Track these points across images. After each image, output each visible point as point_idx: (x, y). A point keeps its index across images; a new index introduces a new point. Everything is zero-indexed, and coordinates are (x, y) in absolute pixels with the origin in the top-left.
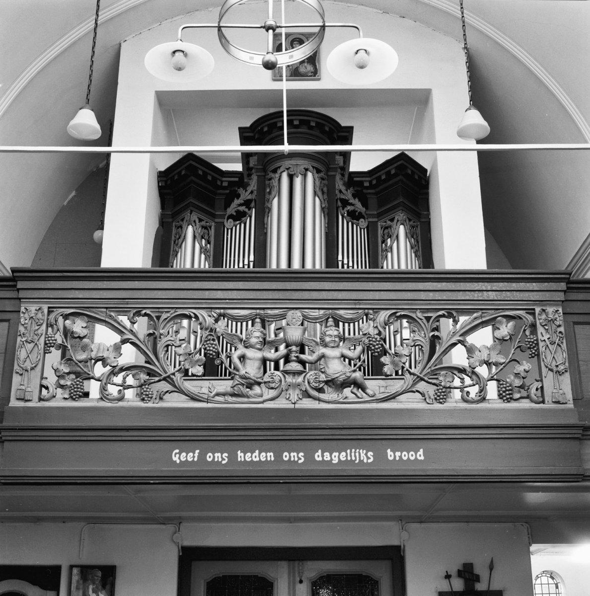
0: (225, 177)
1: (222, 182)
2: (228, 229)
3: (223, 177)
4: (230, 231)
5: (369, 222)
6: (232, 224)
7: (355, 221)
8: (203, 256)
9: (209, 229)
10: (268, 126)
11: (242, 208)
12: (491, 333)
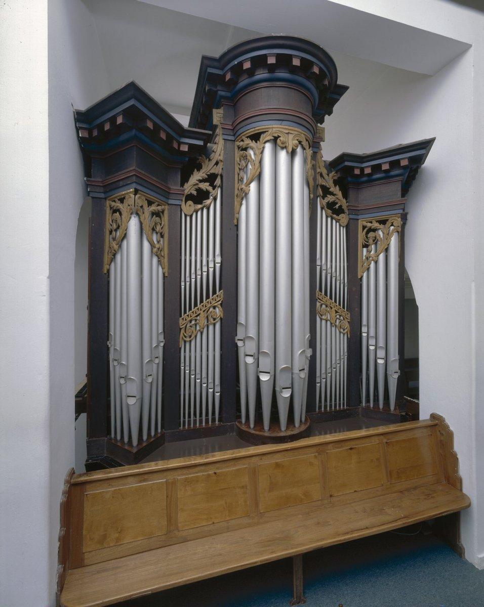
0: (364, 162)
1: (180, 144)
2: (186, 216)
3: (362, 163)
4: (188, 218)
5: (350, 219)
6: (192, 209)
7: (335, 216)
8: (155, 260)
9: (161, 214)
10: (253, 60)
11: (205, 186)
12: (74, 124)
